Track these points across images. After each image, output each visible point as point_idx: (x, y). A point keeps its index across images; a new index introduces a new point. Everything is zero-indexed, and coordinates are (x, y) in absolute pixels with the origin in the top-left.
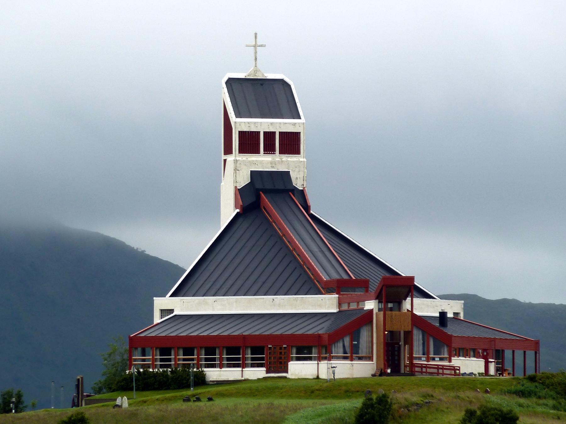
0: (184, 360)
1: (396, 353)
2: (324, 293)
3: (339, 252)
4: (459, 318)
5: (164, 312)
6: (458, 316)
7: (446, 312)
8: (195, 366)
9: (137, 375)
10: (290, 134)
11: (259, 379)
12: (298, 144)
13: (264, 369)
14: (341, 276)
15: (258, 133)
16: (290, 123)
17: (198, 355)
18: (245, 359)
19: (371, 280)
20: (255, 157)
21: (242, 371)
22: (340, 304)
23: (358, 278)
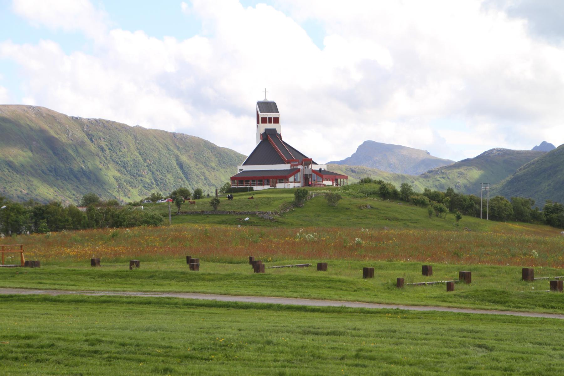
5: (241, 170)
11: (268, 189)
15: (267, 118)
22: (291, 167)
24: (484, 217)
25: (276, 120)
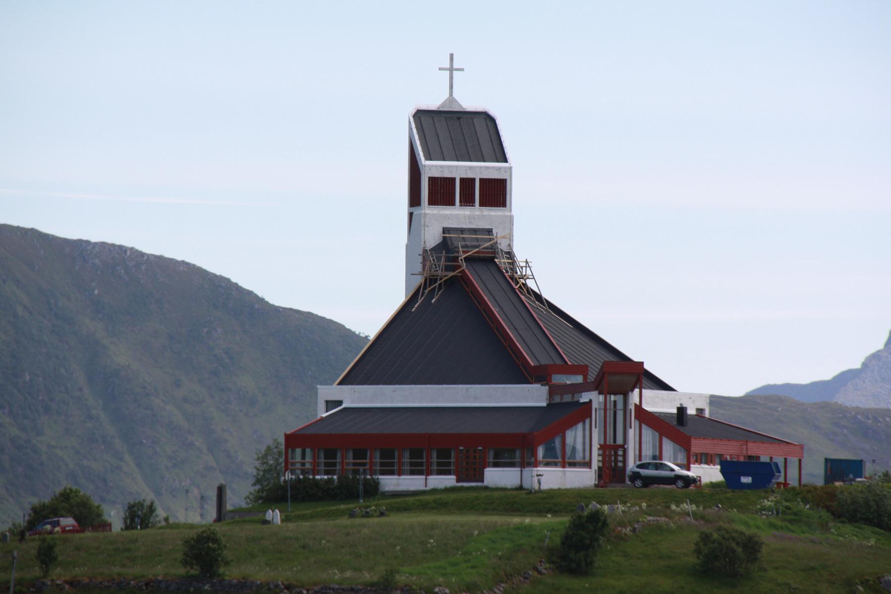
0: (354, 464)
1: (620, 458)
2: (531, 381)
3: (550, 328)
4: (703, 415)
5: (330, 404)
6: (702, 413)
7: (686, 408)
8: (368, 472)
9: (336, 484)
10: (493, 182)
12: (503, 195)
13: (454, 477)
14: (539, 362)
15: (454, 179)
16: (493, 168)
17: (371, 458)
18: (429, 464)
19: (590, 365)
20: (494, 212)
21: (426, 479)
23: (576, 364)
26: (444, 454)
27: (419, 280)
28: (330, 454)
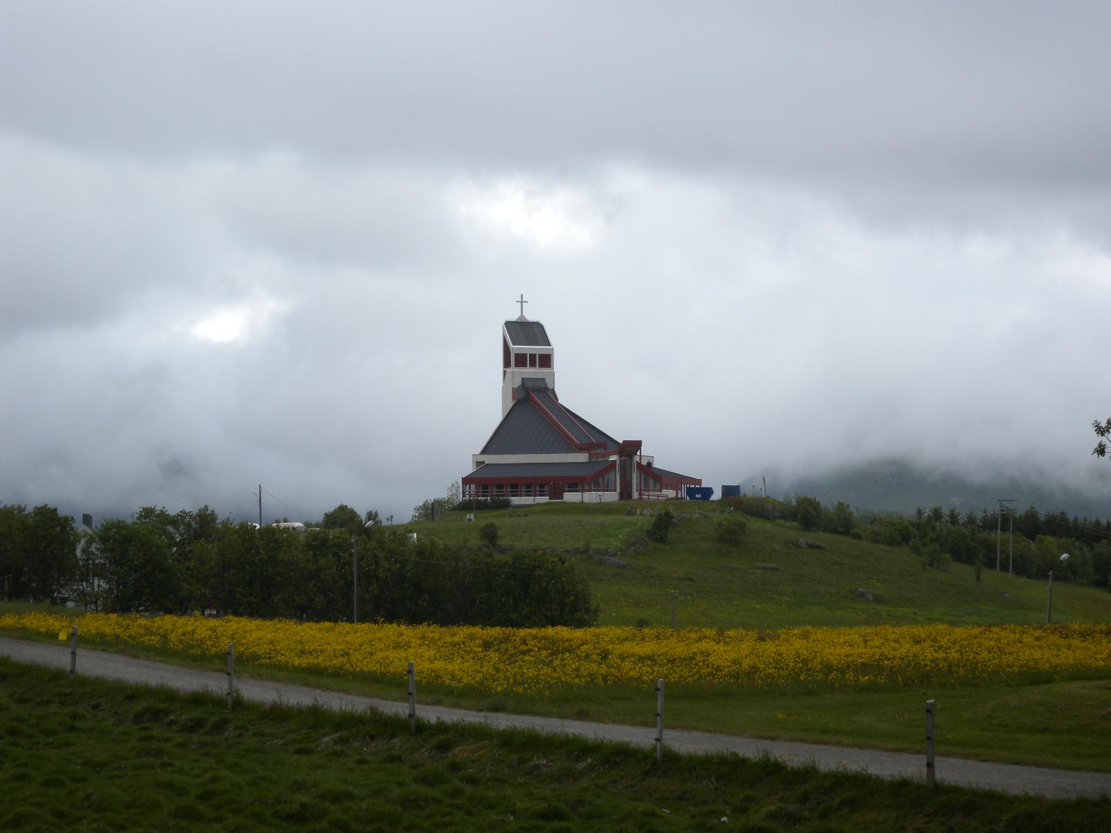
24: (1004, 568)
25: (546, 361)
26: (542, 486)
27: (511, 404)
28: (485, 487)
